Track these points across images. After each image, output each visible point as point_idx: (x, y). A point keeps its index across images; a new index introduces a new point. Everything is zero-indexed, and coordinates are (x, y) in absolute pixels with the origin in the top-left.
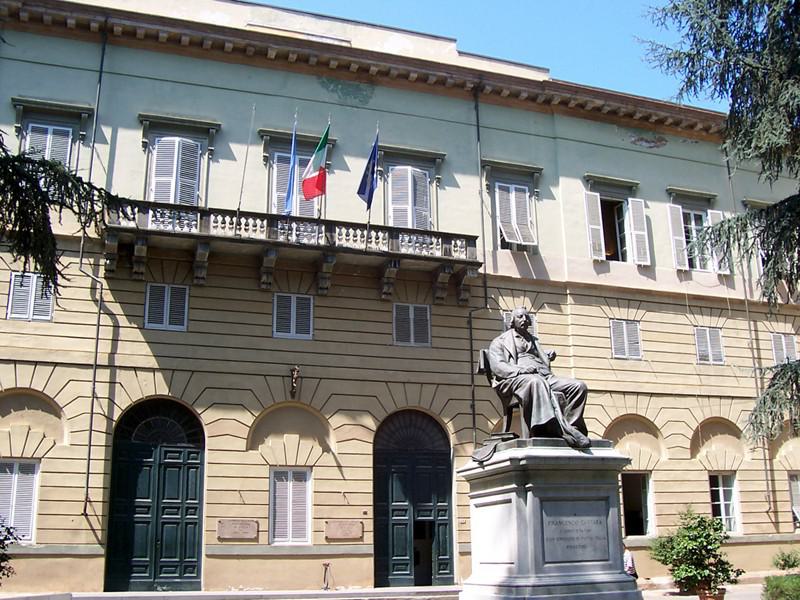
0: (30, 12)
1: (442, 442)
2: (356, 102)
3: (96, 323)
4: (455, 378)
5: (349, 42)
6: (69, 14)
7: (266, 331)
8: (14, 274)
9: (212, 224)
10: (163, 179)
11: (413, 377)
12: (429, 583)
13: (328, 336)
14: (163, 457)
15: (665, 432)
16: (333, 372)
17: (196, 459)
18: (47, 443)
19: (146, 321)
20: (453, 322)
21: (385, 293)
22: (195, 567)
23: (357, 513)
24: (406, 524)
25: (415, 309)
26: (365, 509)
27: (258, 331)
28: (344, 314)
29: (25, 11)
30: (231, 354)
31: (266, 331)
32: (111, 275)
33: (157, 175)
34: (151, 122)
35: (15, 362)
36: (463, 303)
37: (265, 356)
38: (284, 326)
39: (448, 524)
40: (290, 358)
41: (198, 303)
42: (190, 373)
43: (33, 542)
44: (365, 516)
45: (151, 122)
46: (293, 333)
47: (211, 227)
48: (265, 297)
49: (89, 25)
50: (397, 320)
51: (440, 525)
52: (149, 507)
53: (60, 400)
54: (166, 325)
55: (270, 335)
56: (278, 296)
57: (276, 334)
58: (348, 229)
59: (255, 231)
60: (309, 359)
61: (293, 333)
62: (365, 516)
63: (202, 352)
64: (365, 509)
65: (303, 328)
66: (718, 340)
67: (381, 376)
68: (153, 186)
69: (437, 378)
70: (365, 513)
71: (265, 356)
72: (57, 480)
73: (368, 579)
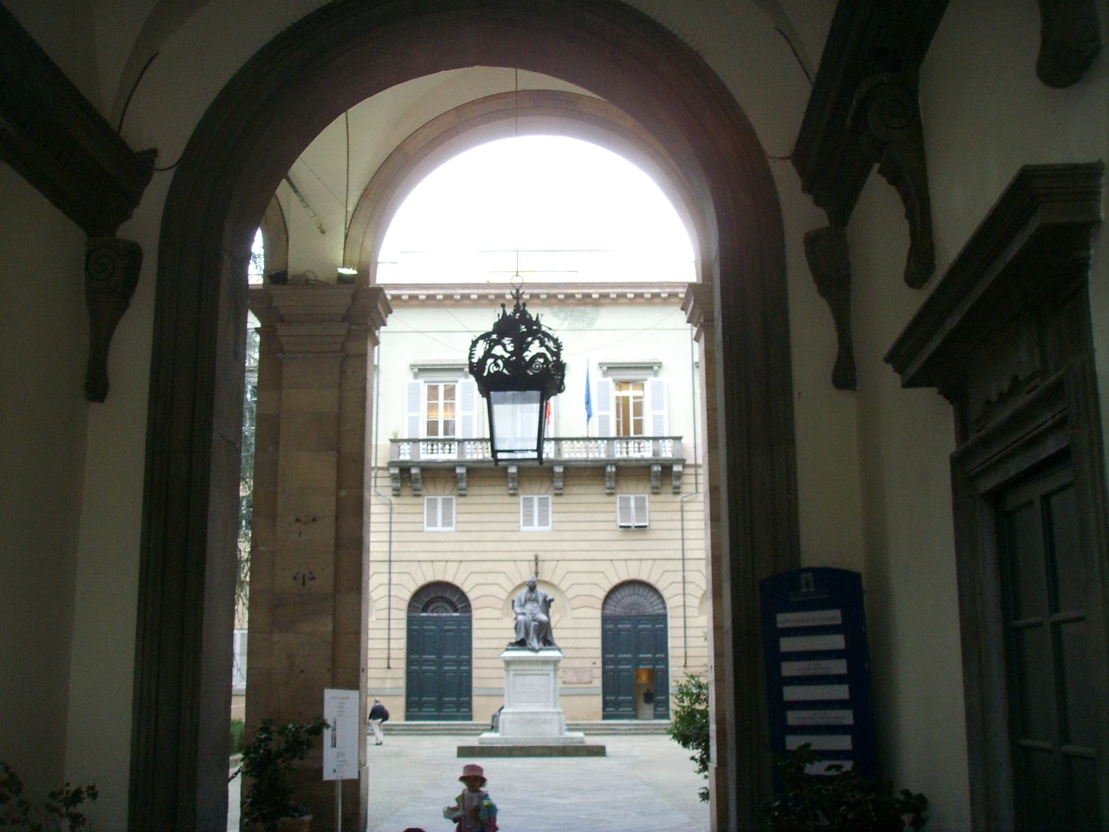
1: (661, 606)
2: (582, 325)
4: (671, 554)
7: (418, 527)
10: (657, 413)
11: (633, 555)
13: (467, 527)
15: (569, 594)
16: (569, 555)
20: (670, 507)
22: (469, 705)
23: (588, 664)
25: (636, 498)
27: (508, 527)
28: (575, 508)
30: (489, 546)
31: (418, 527)
36: (677, 491)
37: (515, 546)
38: (432, 522)
40: (534, 546)
41: (464, 509)
42: (651, 562)
48: (514, 499)
49: (435, 297)
50: (621, 508)
52: (434, 661)
53: (563, 587)
54: (439, 528)
55: (421, 529)
56: (524, 498)
57: (427, 529)
60: (549, 546)
63: (467, 546)
64: (594, 660)
65: (447, 523)
67: (608, 556)
69: (654, 555)
70: (594, 663)
71: (515, 546)
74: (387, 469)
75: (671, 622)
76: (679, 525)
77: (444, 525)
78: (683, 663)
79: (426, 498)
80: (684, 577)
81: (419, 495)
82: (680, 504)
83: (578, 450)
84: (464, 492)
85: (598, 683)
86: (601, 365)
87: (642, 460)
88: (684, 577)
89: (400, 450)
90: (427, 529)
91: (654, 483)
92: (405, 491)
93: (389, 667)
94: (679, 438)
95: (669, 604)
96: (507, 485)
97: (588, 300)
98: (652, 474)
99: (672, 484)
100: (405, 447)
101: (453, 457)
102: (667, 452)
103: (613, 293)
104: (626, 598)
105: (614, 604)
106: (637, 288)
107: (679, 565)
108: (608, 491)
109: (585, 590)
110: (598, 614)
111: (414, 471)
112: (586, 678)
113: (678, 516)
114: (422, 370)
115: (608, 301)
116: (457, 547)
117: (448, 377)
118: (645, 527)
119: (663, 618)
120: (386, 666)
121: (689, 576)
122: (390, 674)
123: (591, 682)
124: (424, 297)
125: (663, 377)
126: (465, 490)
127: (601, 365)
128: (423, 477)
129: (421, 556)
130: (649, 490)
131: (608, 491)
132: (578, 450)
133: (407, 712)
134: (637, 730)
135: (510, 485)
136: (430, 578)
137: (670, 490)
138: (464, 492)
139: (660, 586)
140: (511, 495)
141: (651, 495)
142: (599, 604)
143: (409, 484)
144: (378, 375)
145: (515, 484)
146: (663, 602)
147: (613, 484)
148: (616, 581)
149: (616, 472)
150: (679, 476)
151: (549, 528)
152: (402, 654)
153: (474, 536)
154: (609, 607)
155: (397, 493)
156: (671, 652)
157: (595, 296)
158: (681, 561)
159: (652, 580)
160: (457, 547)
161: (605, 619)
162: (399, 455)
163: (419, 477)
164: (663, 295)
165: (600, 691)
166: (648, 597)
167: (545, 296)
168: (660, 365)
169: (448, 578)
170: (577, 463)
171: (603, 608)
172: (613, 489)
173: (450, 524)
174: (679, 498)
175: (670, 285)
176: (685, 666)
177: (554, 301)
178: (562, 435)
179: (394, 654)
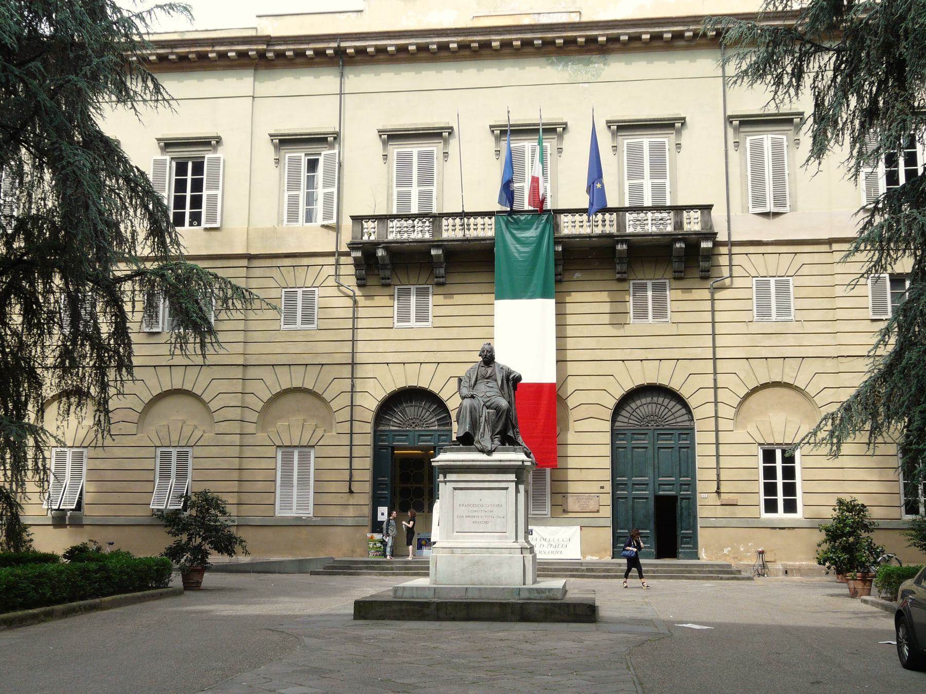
0: (275, 51)
1: (686, 417)
3: (351, 327)
4: (698, 353)
5: (256, 29)
6: (209, 49)
7: (387, 323)
8: (754, 279)
9: (444, 228)
12: (674, 555)
14: (416, 441)
17: (686, 440)
18: (319, 433)
19: (396, 321)
20: (696, 294)
21: (618, 273)
23: (595, 488)
24: (646, 498)
26: (602, 484)
29: (270, 51)
31: (387, 323)
32: (363, 282)
33: (398, 186)
34: (388, 135)
35: (290, 365)
36: (706, 276)
38: (404, 316)
39: (691, 500)
43: (311, 515)
44: (602, 491)
45: (388, 135)
46: (299, 325)
47: (443, 231)
49: (512, 43)
51: (682, 499)
54: (413, 323)
58: (604, 215)
59: (455, 230)
61: (413, 323)
62: (602, 491)
64: (602, 484)
66: (787, 291)
68: (395, 197)
70: (602, 487)
72: (328, 463)
73: (606, 550)
74: (347, 254)
75: (699, 438)
76: (708, 317)
77: (418, 320)
78: (715, 489)
79: (632, 282)
80: (715, 380)
81: (389, 285)
82: (136, 310)
83: (405, 229)
84: (388, 281)
85: (607, 512)
86: (609, 123)
87: (603, 236)
88: (715, 380)
89: (362, 228)
90: (397, 324)
91: (676, 265)
92: (371, 281)
93: (351, 492)
94: (709, 207)
95: (697, 414)
96: (615, 269)
97: (593, 46)
98: (674, 254)
99: (699, 266)
100: (369, 225)
101: (611, 229)
102: (693, 223)
103: (667, 32)
104: (644, 407)
105: (628, 415)
106: (655, 27)
107: (346, 371)
108: (618, 276)
109: (592, 397)
110: (607, 426)
111: (380, 253)
112: (592, 505)
113: (707, 305)
114: (393, 136)
115: (617, 46)
116: (434, 345)
117: (313, 149)
118: (159, 333)
119: (689, 432)
120: (348, 491)
121: (722, 380)
122: (354, 500)
123: (598, 511)
124: (393, 48)
125: (221, 153)
126: (389, 279)
127: (609, 123)
128: (392, 264)
129: (391, 358)
130: (669, 274)
131: (618, 276)
132: (405, 229)
133: (613, 548)
134: (654, 572)
135: (618, 267)
136: (401, 384)
137: (698, 274)
138: (388, 281)
139: (685, 393)
140: (619, 280)
141: (435, 287)
142: (608, 415)
143: (376, 272)
144: (340, 145)
145: (625, 267)
146: (689, 412)
147: (625, 267)
148: (629, 386)
149: (628, 250)
150: (710, 255)
151: (429, 324)
152: (368, 476)
153: (454, 333)
154: (620, 418)
155: (362, 283)
156: (699, 475)
157: (602, 39)
158: (350, 366)
159: (675, 385)
160: (434, 345)
161: (615, 434)
162: (362, 235)
163: (387, 261)
164: (687, 34)
165: (609, 522)
166: (670, 407)
167: (519, 43)
168: (683, 121)
169: (423, 384)
170: (472, 243)
171: (614, 420)
172: (625, 273)
173: (311, 322)
174: (710, 283)
175: (696, 19)
176: (718, 492)
177: (551, 48)
178: (681, 203)
179: (357, 476)
